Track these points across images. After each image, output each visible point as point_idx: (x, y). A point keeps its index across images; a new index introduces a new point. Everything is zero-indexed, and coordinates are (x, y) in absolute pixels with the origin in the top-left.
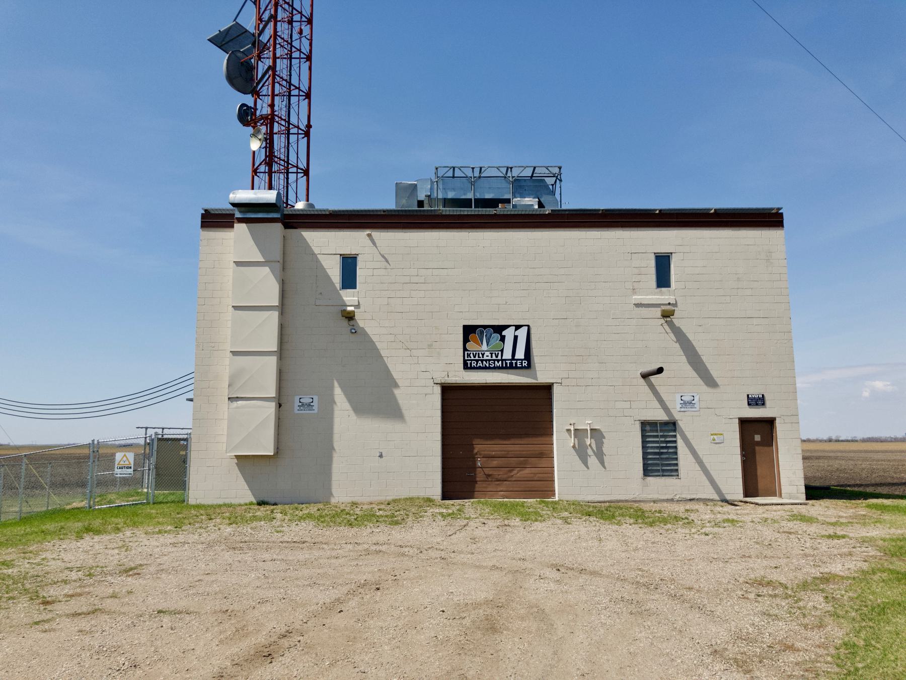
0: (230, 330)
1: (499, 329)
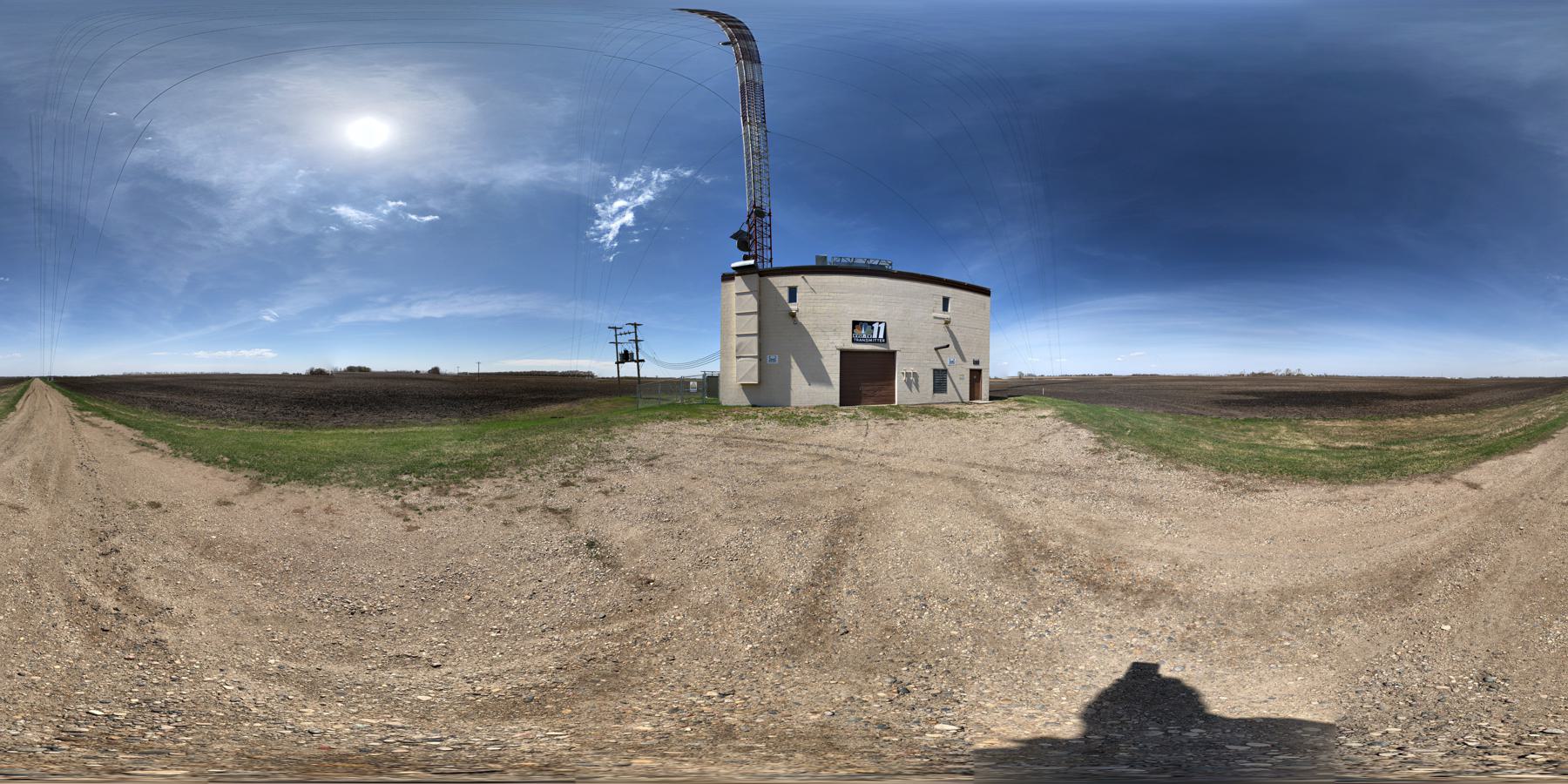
0: (734, 325)
1: (871, 323)
